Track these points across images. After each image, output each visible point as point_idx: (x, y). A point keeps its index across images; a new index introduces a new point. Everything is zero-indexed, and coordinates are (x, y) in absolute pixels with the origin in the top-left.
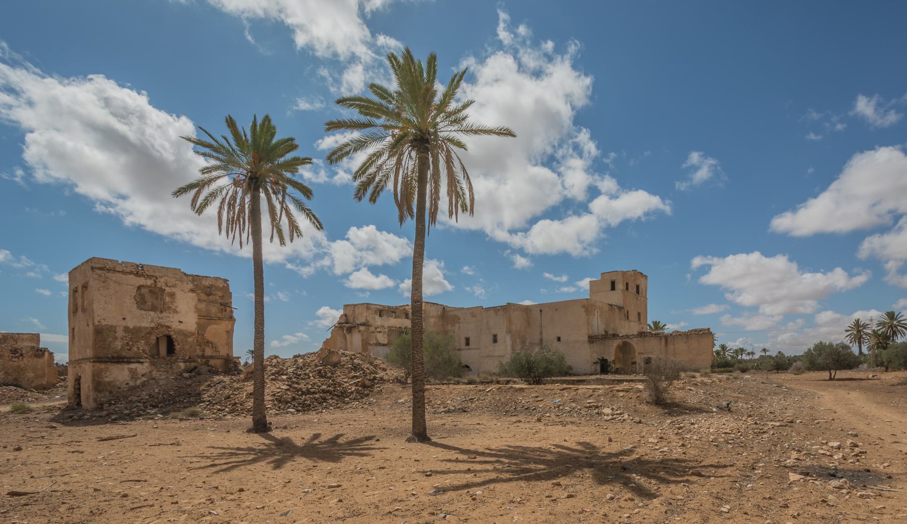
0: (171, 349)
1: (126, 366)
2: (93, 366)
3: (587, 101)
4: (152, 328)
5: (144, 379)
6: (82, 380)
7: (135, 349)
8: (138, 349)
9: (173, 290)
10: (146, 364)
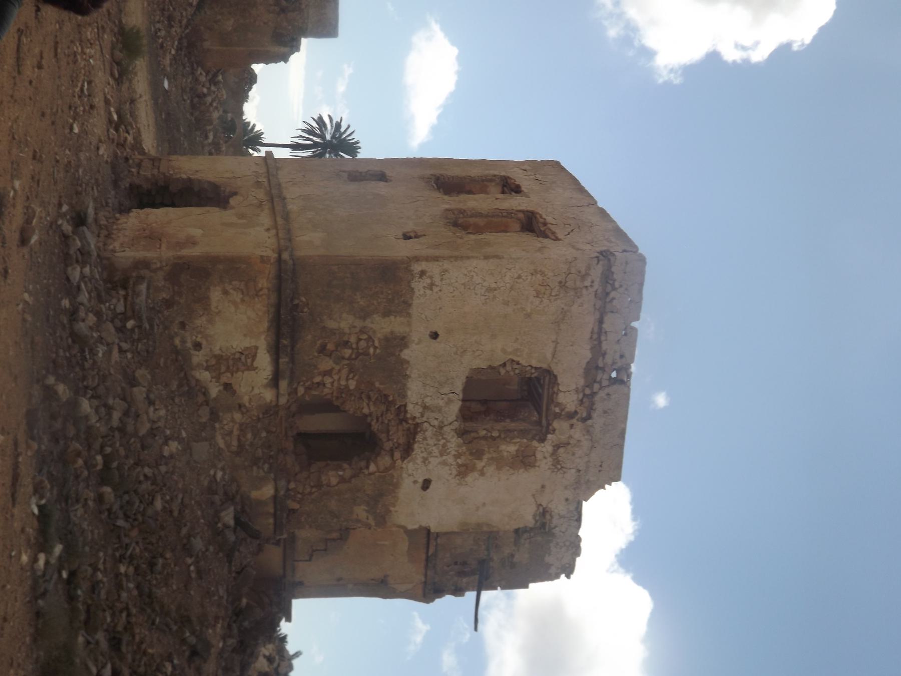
0: (319, 449)
1: (262, 344)
2: (264, 260)
3: (634, 523)
4: (402, 409)
5: (214, 391)
6: (214, 215)
7: (326, 364)
8: (328, 373)
9: (544, 465)
10: (269, 395)
